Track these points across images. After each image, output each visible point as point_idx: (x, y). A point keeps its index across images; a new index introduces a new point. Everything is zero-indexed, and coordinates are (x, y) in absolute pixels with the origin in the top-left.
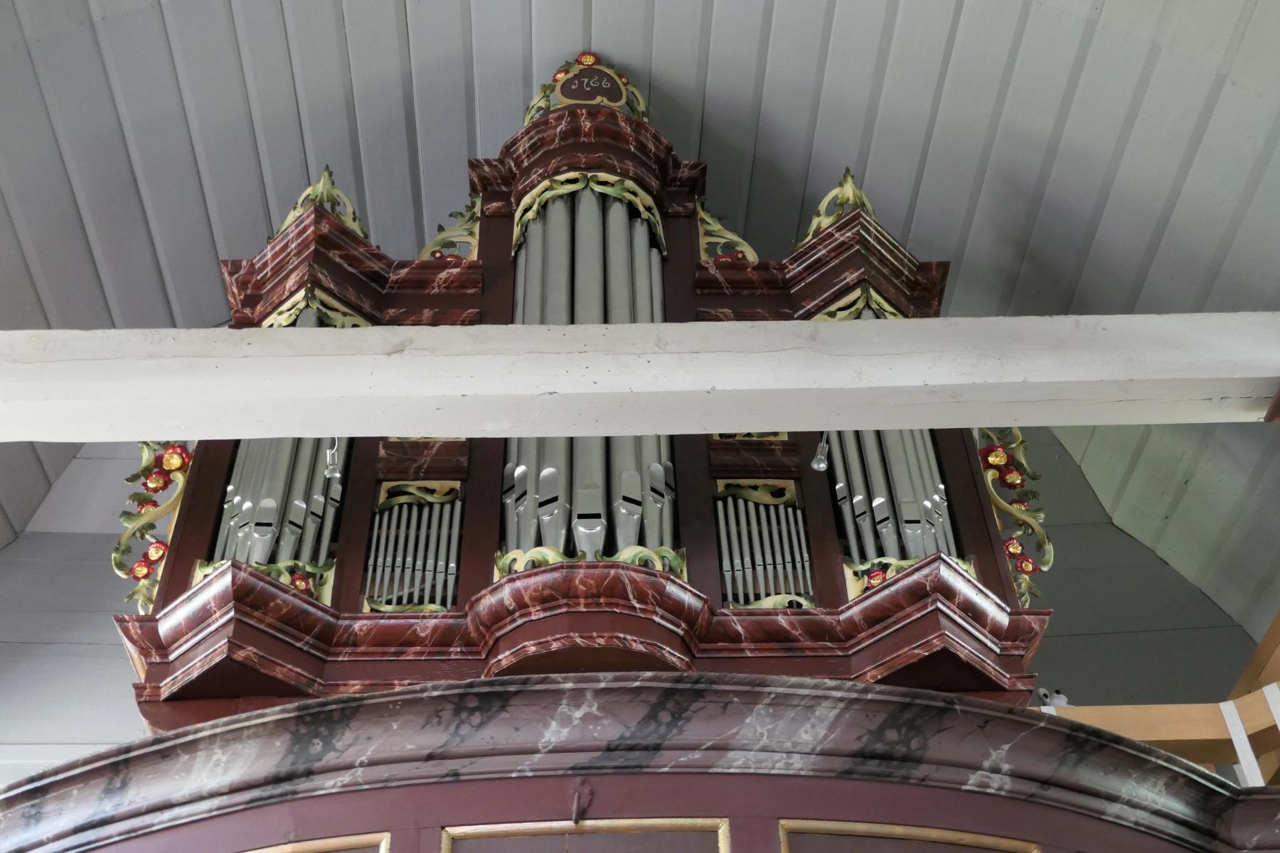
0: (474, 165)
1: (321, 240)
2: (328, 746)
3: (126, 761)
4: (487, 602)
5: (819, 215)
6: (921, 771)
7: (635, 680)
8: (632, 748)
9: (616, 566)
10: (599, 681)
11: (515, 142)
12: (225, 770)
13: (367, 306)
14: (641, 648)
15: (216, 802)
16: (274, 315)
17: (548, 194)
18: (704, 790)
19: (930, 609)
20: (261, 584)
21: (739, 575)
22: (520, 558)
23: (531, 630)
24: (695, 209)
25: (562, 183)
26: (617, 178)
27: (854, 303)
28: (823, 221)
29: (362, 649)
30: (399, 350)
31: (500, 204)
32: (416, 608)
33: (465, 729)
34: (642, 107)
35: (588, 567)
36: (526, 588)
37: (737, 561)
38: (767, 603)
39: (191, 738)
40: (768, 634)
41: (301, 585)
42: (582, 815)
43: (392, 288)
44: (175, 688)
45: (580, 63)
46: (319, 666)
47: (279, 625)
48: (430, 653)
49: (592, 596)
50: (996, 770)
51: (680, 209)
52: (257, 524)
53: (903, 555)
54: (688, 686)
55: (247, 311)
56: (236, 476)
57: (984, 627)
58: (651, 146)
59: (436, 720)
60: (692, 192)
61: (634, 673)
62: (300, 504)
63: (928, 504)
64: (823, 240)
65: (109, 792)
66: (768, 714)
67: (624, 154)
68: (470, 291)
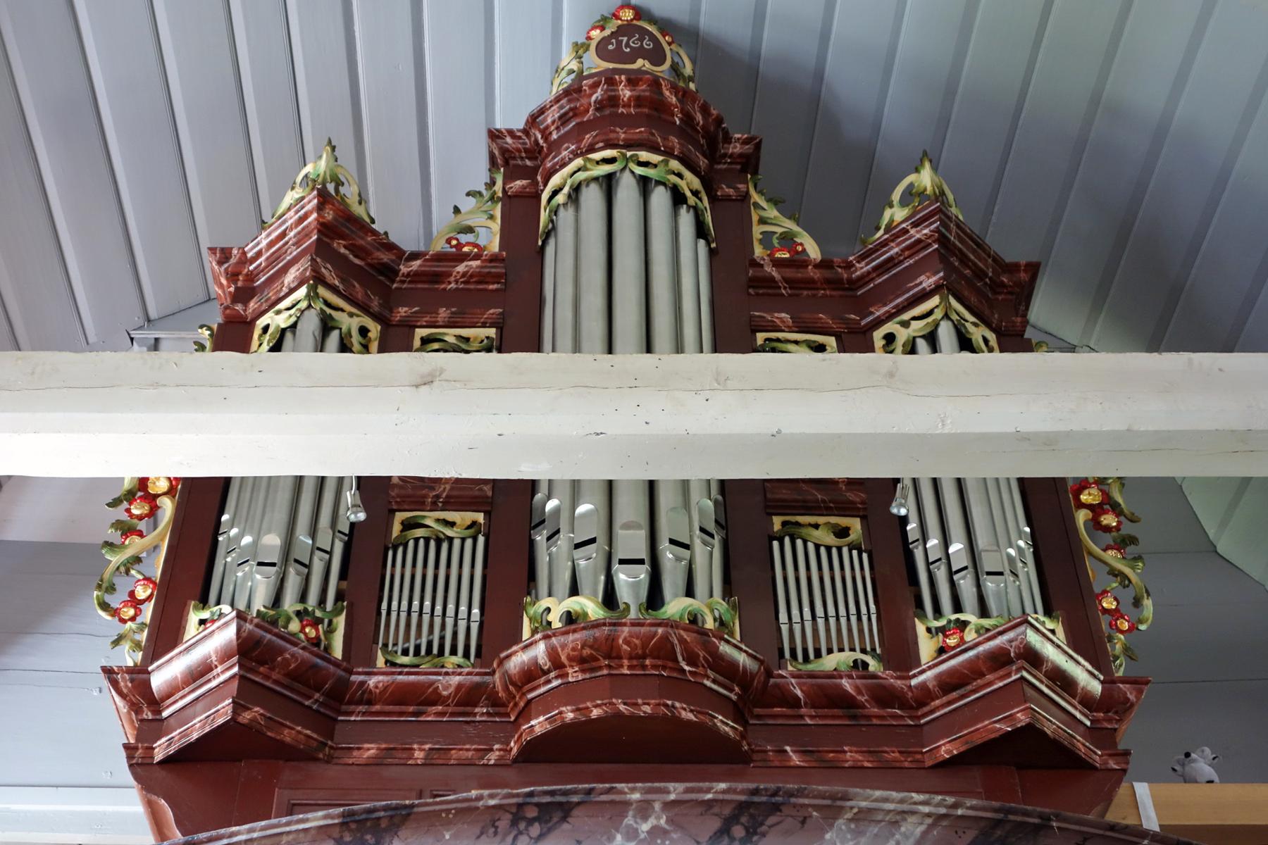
0: (494, 135)
1: (325, 229)
4: (518, 660)
5: (891, 206)
7: (708, 791)
10: (669, 792)
11: (542, 111)
14: (691, 716)
16: (270, 314)
17: (581, 176)
19: (1014, 677)
20: (269, 636)
21: (797, 628)
22: (556, 607)
24: (747, 192)
25: (598, 163)
26: (661, 158)
27: (930, 313)
28: (897, 214)
29: (377, 708)
30: (427, 381)
31: (524, 182)
32: (436, 660)
34: (688, 70)
35: (633, 625)
37: (795, 612)
40: (828, 696)
43: (403, 282)
44: (172, 750)
45: (618, 18)
48: (452, 714)
49: (637, 657)
51: (731, 191)
52: (260, 564)
53: (984, 612)
54: (764, 799)
55: (239, 307)
57: (1074, 697)
58: (699, 117)
59: (493, 830)
60: (744, 171)
61: (707, 784)
62: (303, 538)
63: (1012, 552)
64: (897, 236)
66: (850, 831)
68: (491, 287)
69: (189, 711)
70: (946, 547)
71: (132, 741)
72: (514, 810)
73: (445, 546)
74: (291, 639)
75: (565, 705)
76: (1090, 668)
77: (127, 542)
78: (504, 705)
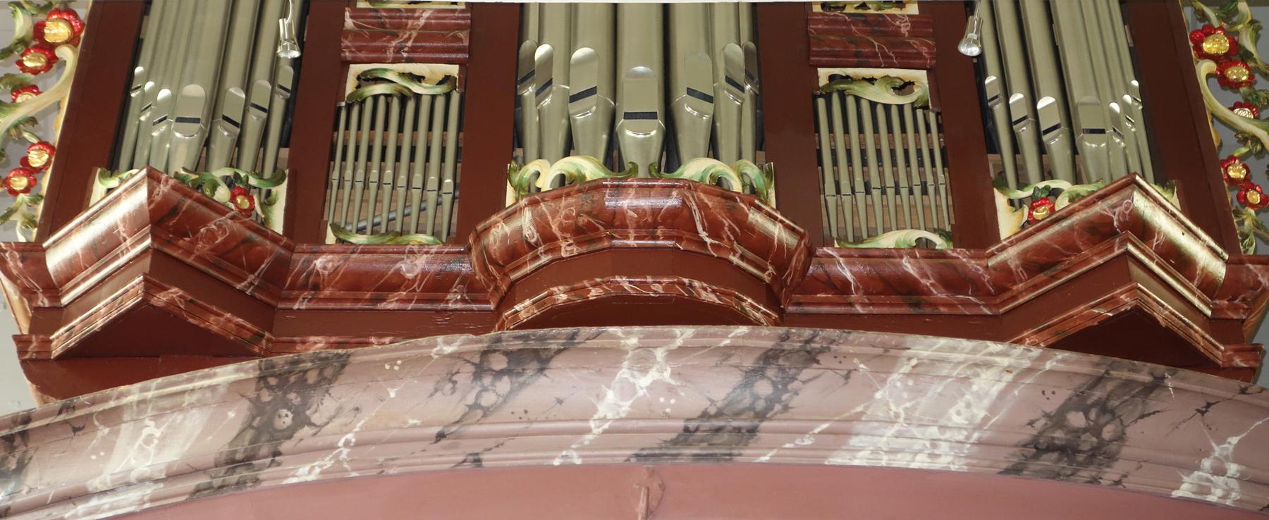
4: (499, 232)
14: (712, 298)
44: (71, 343)
52: (180, 120)
57: (1191, 280)
59: (450, 385)
62: (235, 92)
63: (1116, 107)
69: (92, 297)
70: (1034, 102)
71: (25, 332)
72: (477, 360)
74: (220, 209)
75: (557, 285)
76: (1213, 244)
77: (19, 100)
78: (483, 290)
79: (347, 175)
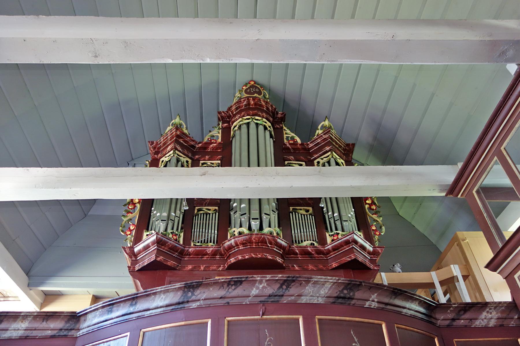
2: (193, 294)
3: (137, 297)
4: (227, 244)
6: (353, 302)
7: (277, 277)
8: (276, 296)
9: (263, 234)
11: (231, 107)
12: (165, 300)
13: (190, 155)
14: (271, 258)
15: (162, 309)
16: (164, 158)
17: (241, 123)
18: (296, 307)
21: (297, 235)
22: (236, 230)
23: (239, 252)
27: (328, 156)
30: (204, 174)
32: (207, 244)
33: (230, 290)
34: (267, 97)
36: (238, 240)
37: (296, 231)
38: (305, 244)
39: (155, 291)
40: (305, 252)
41: (175, 237)
42: (263, 315)
46: (179, 261)
47: (169, 250)
50: (373, 301)
53: (343, 230)
55: (156, 156)
56: (154, 206)
58: (270, 108)
63: (350, 215)
65: (131, 305)
67: (262, 111)
69: (144, 258)
73: (208, 215)
74: (170, 239)
79: (196, 231)
